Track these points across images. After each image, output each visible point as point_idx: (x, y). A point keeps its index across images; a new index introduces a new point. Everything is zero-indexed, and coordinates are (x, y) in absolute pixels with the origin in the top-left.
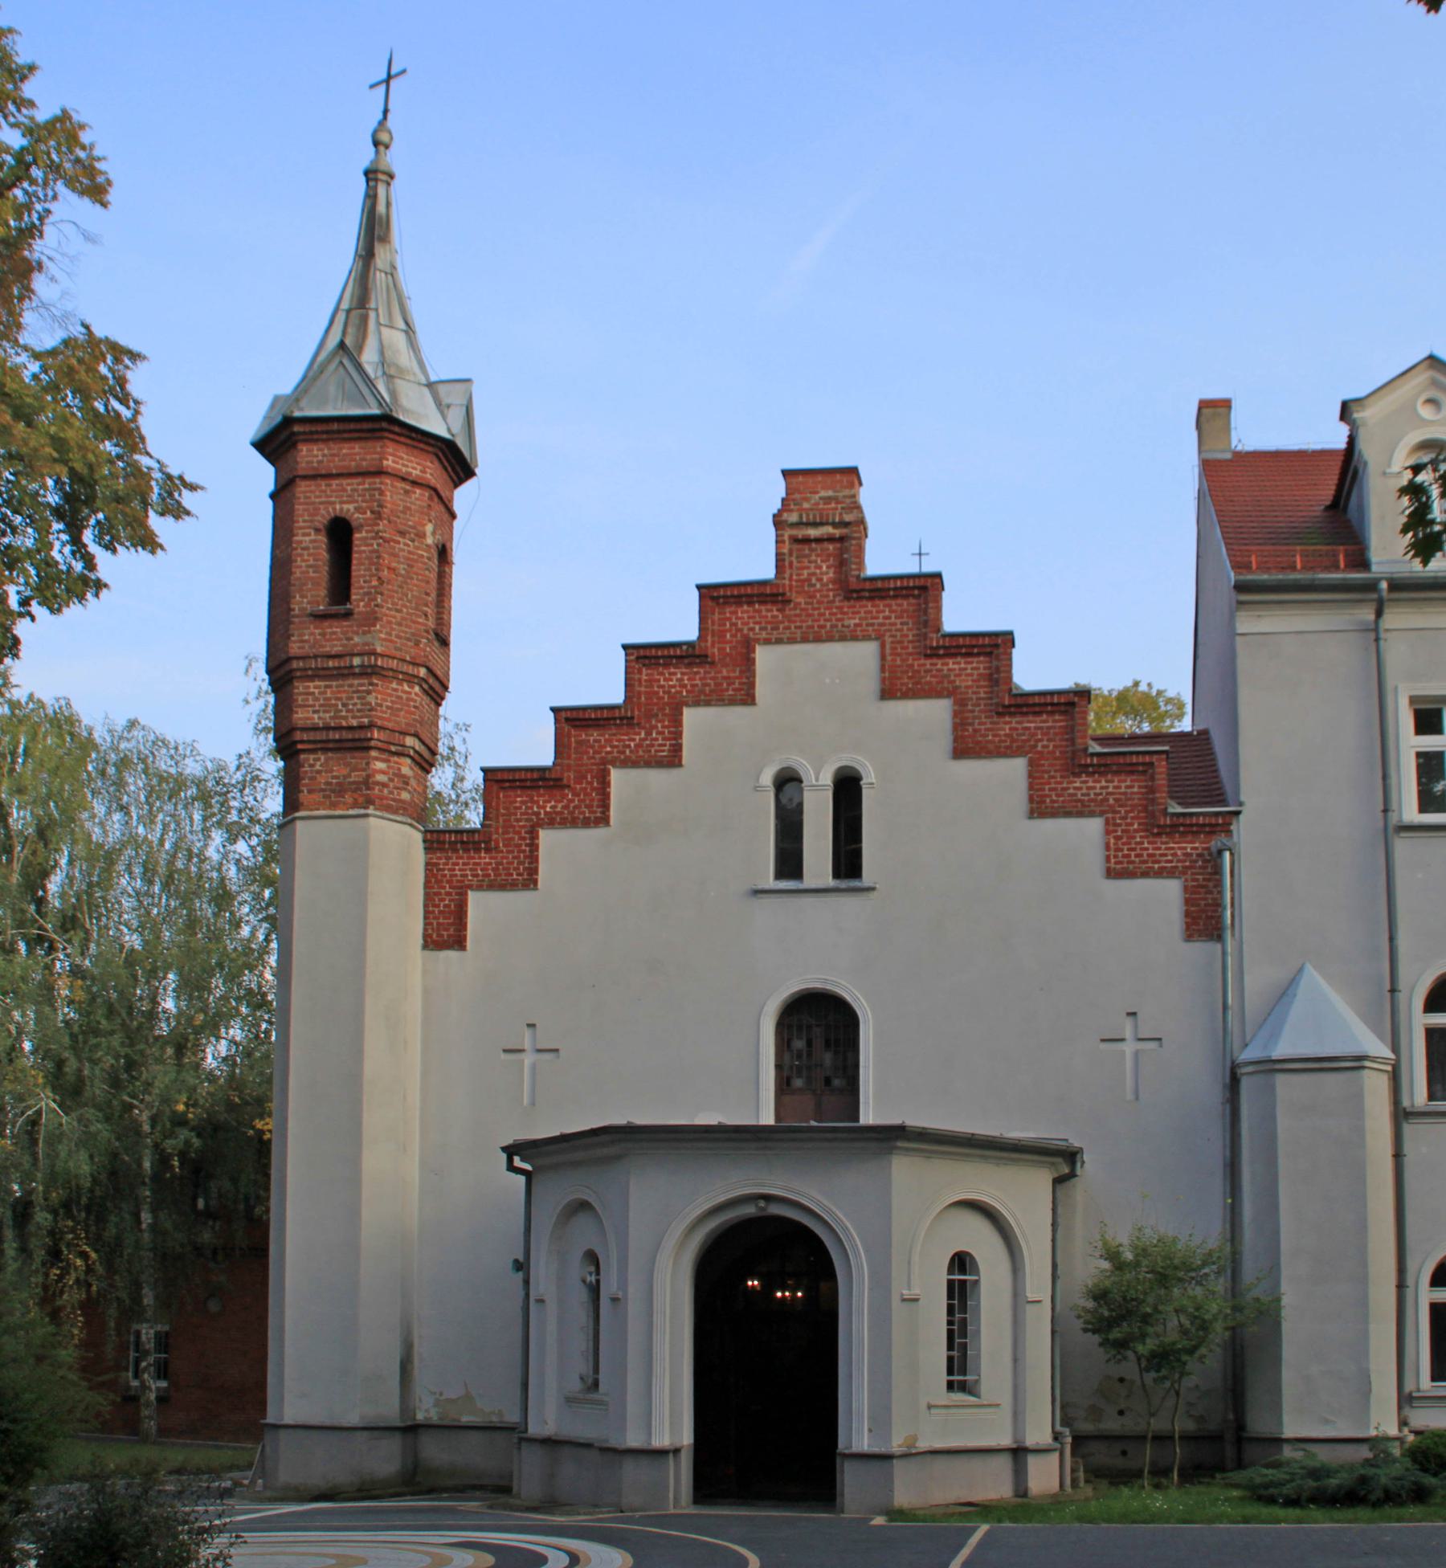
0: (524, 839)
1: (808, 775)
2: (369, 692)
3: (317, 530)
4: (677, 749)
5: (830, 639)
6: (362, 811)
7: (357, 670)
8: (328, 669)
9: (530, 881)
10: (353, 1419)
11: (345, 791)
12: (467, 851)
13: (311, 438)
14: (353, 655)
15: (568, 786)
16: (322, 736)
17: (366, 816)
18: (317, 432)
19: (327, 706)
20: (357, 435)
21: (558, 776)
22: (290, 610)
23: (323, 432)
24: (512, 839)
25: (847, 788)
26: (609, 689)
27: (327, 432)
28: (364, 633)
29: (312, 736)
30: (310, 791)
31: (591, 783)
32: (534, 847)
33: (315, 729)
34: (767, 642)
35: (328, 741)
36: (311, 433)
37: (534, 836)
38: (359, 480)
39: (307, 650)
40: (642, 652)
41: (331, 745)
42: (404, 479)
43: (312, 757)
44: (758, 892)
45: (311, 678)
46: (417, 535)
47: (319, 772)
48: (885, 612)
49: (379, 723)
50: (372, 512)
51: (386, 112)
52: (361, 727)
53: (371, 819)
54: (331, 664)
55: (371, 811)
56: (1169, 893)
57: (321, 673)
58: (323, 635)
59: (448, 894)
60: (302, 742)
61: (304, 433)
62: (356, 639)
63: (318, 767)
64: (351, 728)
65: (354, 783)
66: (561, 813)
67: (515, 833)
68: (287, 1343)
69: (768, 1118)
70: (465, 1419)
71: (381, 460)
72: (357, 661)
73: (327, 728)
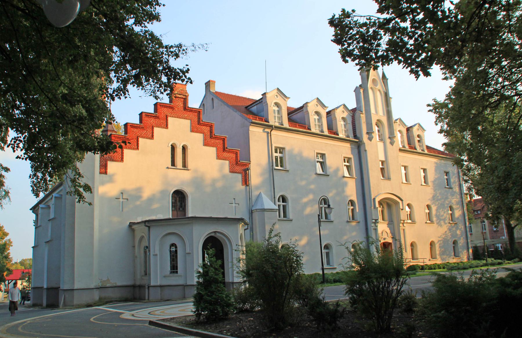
1: (178, 145)
4: (153, 136)
5: (182, 118)
10: (92, 286)
25: (184, 148)
26: (136, 120)
34: (170, 116)
44: (168, 168)
48: (191, 114)
56: (239, 176)
68: (76, 270)
69: (171, 217)
70: (108, 285)
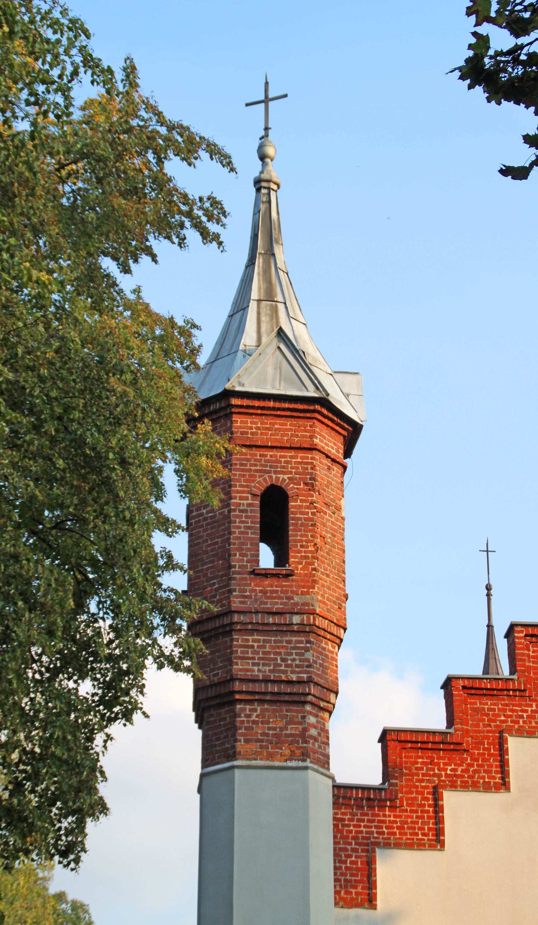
0: (427, 799)
2: (307, 650)
3: (254, 495)
6: (301, 764)
7: (295, 628)
8: (268, 624)
9: (437, 840)
11: (283, 742)
12: (372, 808)
13: (246, 411)
14: (293, 613)
15: (467, 751)
16: (257, 687)
17: (306, 768)
18: (253, 407)
19: (266, 660)
20: (289, 413)
21: (459, 740)
22: (230, 567)
23: (259, 408)
24: (416, 799)
27: (263, 408)
28: (303, 593)
29: (251, 687)
30: (247, 741)
31: (489, 749)
32: (438, 809)
33: (254, 681)
35: (265, 693)
36: (248, 407)
37: (437, 798)
38: (293, 453)
39: (249, 605)
40: (530, 631)
41: (268, 698)
42: (327, 456)
43: (248, 707)
45: (251, 632)
46: (336, 508)
47: (254, 722)
49: (316, 679)
50: (306, 484)
51: (267, 129)
52: (299, 682)
53: (310, 772)
54: (271, 620)
55: (308, 763)
57: (260, 628)
58: (264, 592)
59: (354, 850)
60: (240, 692)
61: (241, 407)
62: (296, 599)
63: (254, 718)
64: (290, 682)
65: (291, 735)
66: (462, 776)
67: (418, 793)
71: (312, 437)
72: (296, 619)
73: (266, 681)
